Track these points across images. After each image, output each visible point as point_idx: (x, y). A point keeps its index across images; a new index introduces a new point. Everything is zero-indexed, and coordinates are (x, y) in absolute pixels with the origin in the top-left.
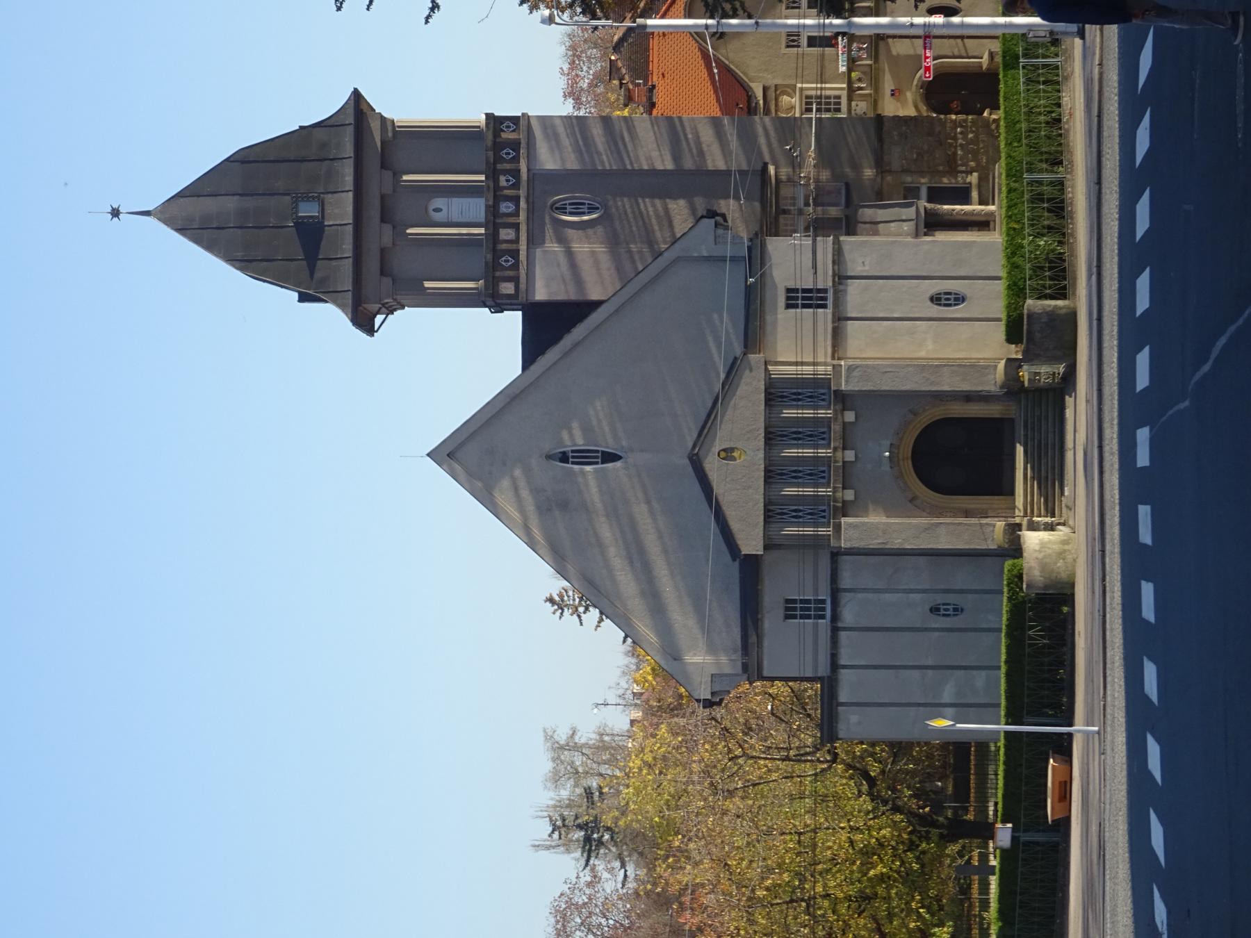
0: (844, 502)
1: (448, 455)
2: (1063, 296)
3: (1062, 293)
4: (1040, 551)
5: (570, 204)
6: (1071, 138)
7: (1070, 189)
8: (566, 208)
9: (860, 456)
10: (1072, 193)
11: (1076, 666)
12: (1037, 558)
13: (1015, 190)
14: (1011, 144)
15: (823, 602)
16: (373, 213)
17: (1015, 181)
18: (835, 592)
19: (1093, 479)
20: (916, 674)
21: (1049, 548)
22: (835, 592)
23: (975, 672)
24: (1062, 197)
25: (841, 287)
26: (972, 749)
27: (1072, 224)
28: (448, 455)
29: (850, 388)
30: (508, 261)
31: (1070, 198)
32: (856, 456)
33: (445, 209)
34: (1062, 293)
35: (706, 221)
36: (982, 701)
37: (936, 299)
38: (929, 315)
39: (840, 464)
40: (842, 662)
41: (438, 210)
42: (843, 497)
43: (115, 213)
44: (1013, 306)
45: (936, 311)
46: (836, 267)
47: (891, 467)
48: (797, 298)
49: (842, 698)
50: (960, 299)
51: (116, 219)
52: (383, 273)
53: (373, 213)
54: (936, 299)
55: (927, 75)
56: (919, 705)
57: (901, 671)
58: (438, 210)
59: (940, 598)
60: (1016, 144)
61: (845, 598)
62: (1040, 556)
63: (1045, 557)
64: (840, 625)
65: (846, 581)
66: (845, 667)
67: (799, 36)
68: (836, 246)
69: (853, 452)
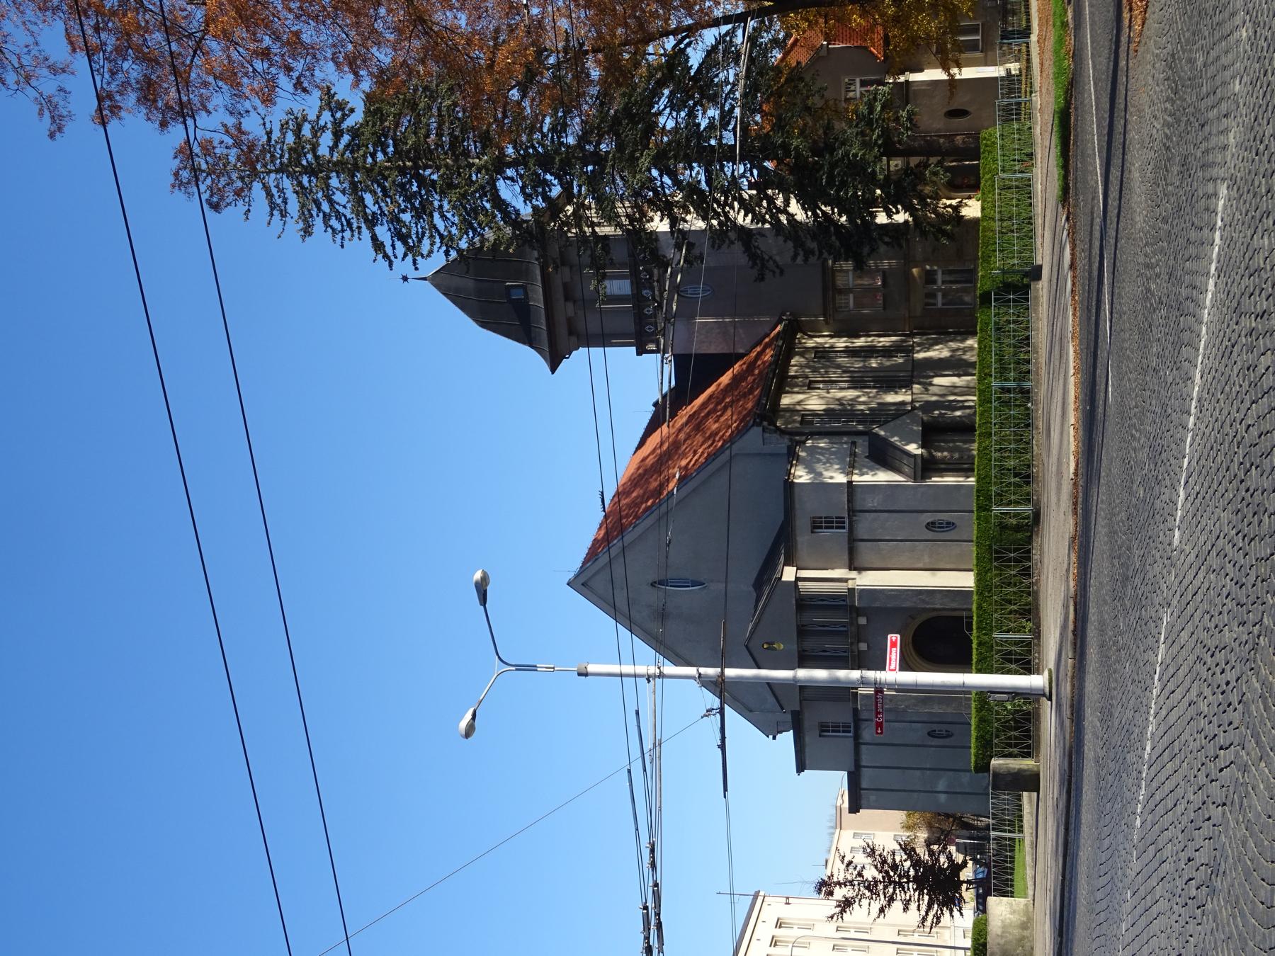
2: (1027, 755)
3: (1028, 751)
4: (1002, 937)
6: (1035, 557)
7: (1036, 655)
10: (1039, 659)
12: (999, 944)
13: (985, 643)
14: (981, 593)
16: (559, 295)
17: (985, 634)
19: (1056, 736)
20: (918, 773)
21: (1010, 934)
23: (961, 773)
24: (1028, 564)
25: (855, 518)
27: (1039, 653)
29: (862, 605)
31: (1037, 664)
34: (1028, 751)
35: (755, 428)
36: (967, 791)
37: (931, 526)
38: (930, 538)
39: (856, 653)
40: (864, 763)
43: (405, 279)
44: (981, 756)
45: (930, 535)
46: (850, 505)
49: (864, 785)
50: (950, 525)
51: (406, 282)
53: (559, 295)
54: (931, 526)
55: (879, 731)
56: (920, 791)
57: (906, 771)
59: (935, 727)
60: (987, 594)
62: (1002, 942)
63: (1006, 942)
64: (861, 741)
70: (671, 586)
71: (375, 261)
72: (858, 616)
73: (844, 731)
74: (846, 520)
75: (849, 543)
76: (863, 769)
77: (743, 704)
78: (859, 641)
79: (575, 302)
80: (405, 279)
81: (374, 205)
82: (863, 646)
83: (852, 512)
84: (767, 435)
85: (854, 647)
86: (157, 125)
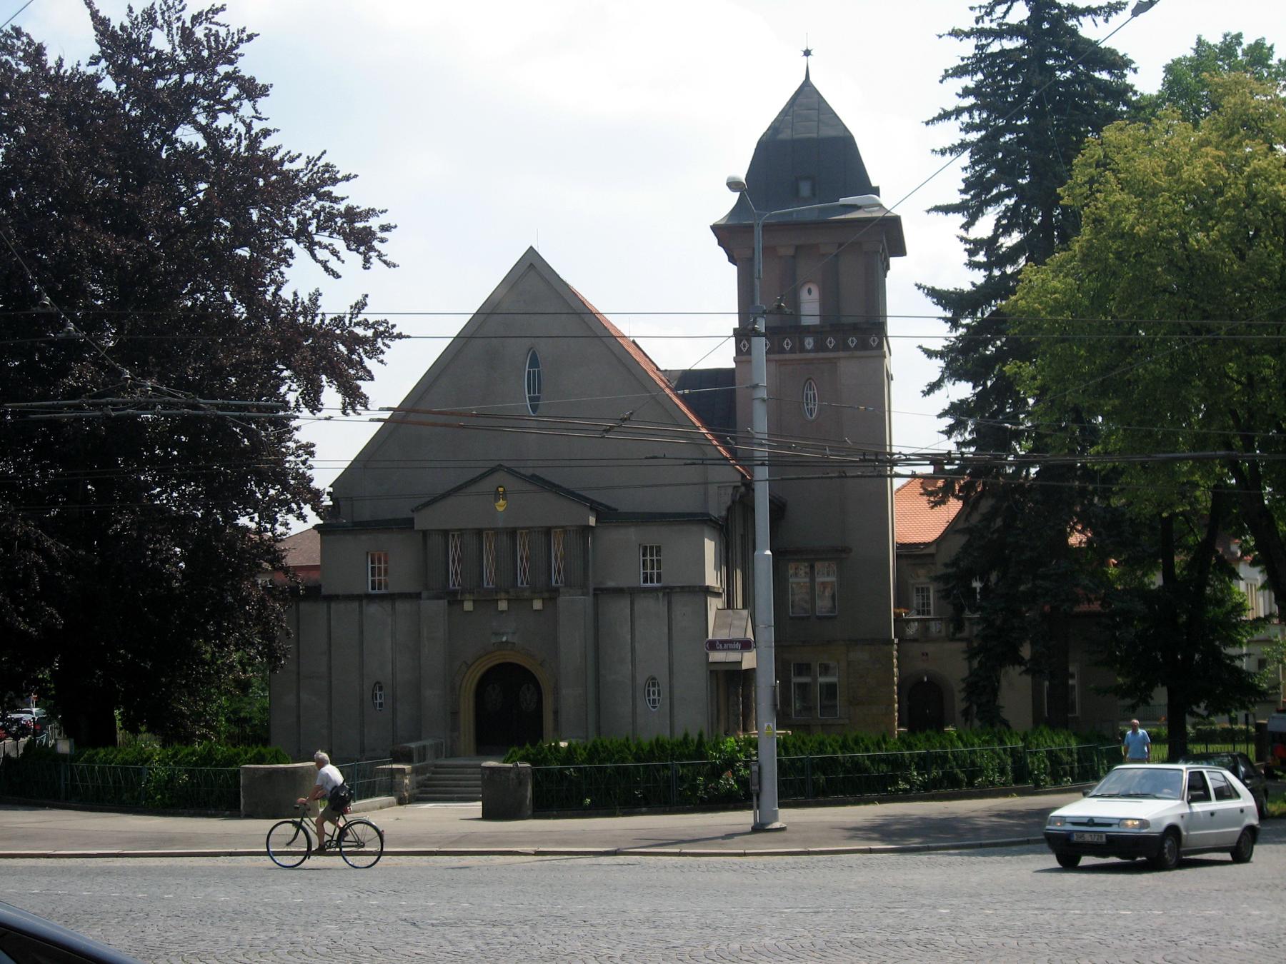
0: (462, 602)
1: (531, 264)
5: (814, 394)
8: (810, 390)
9: (504, 615)
11: (122, 815)
15: (386, 587)
18: (392, 597)
22: (392, 597)
25: (661, 595)
26: (980, 780)
28: (531, 264)
30: (787, 345)
32: (502, 612)
33: (810, 297)
40: (333, 605)
41: (810, 291)
42: (500, 599)
46: (678, 590)
47: (494, 644)
48: (652, 555)
51: (812, 53)
52: (797, 248)
58: (810, 291)
61: (387, 606)
65: (401, 606)
66: (329, 608)
67: (646, 547)
68: (697, 589)
69: (506, 609)
70: (529, 372)
71: (971, 8)
72: (543, 599)
73: (373, 568)
74: (659, 585)
75: (629, 588)
76: (325, 605)
77: (337, 869)
78: (509, 600)
79: (794, 257)
80: (807, 53)
81: (217, 31)
82: (503, 605)
83: (668, 592)
84: (730, 491)
85: (503, 595)
86: (262, 103)
